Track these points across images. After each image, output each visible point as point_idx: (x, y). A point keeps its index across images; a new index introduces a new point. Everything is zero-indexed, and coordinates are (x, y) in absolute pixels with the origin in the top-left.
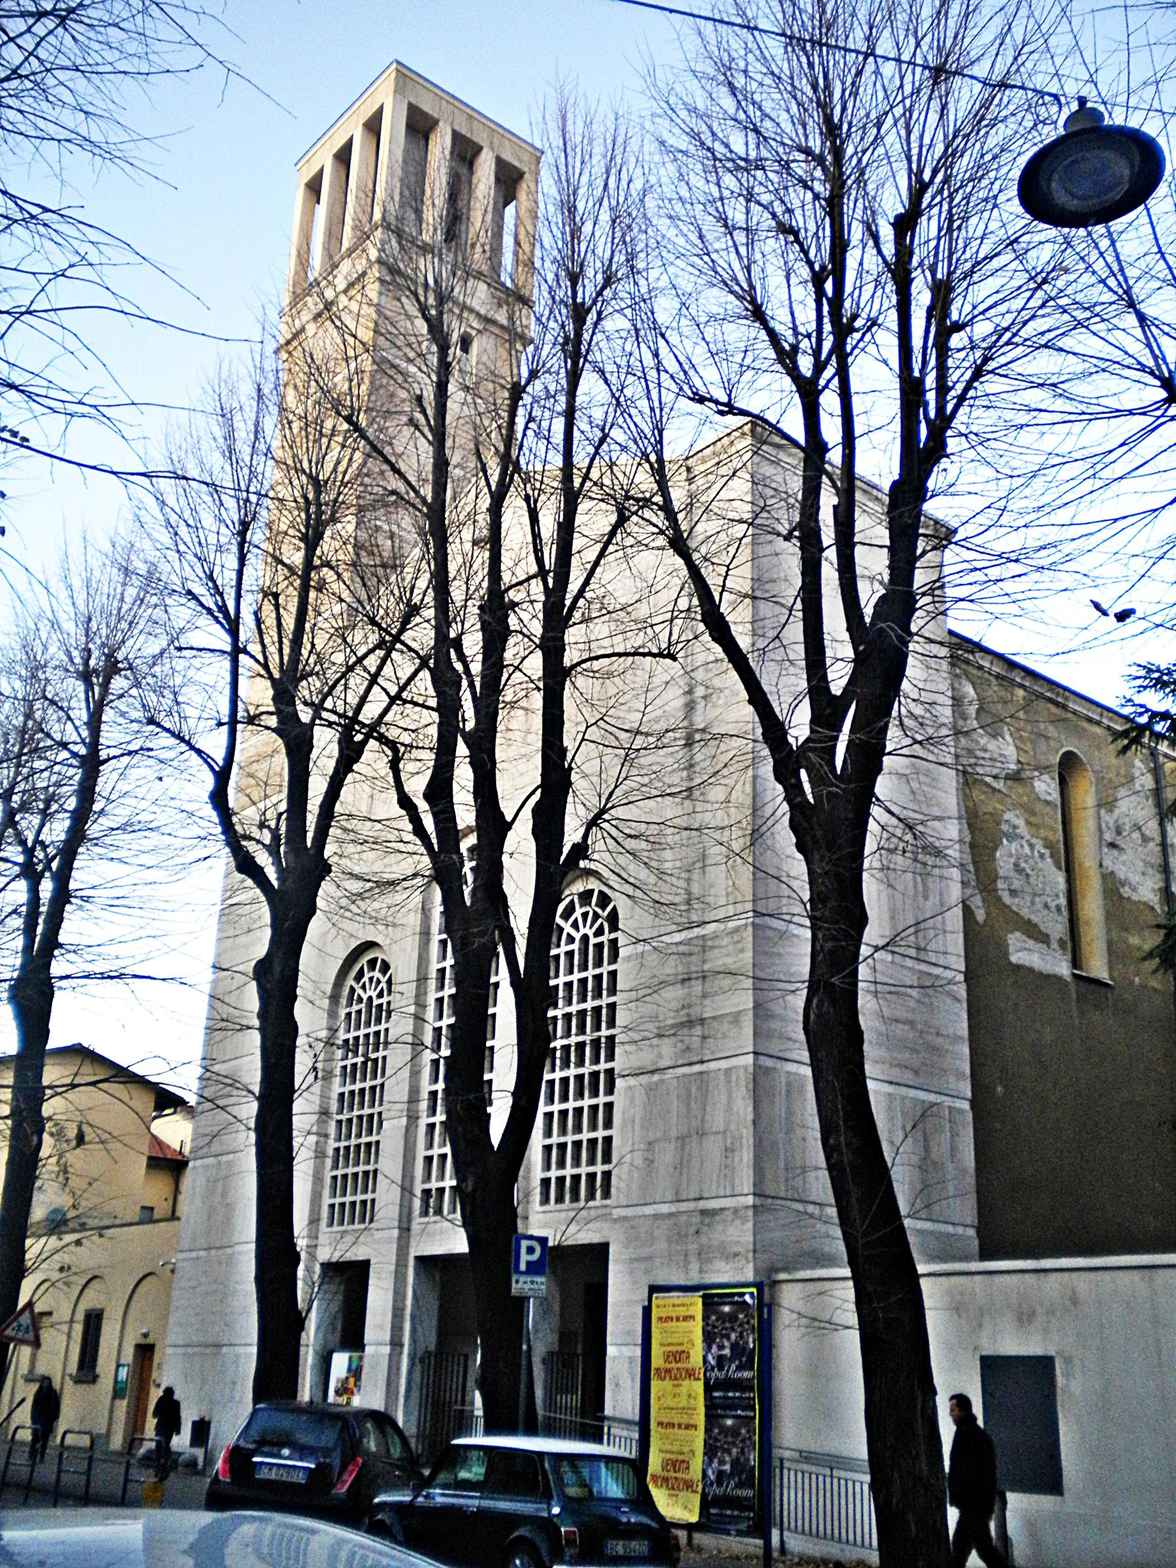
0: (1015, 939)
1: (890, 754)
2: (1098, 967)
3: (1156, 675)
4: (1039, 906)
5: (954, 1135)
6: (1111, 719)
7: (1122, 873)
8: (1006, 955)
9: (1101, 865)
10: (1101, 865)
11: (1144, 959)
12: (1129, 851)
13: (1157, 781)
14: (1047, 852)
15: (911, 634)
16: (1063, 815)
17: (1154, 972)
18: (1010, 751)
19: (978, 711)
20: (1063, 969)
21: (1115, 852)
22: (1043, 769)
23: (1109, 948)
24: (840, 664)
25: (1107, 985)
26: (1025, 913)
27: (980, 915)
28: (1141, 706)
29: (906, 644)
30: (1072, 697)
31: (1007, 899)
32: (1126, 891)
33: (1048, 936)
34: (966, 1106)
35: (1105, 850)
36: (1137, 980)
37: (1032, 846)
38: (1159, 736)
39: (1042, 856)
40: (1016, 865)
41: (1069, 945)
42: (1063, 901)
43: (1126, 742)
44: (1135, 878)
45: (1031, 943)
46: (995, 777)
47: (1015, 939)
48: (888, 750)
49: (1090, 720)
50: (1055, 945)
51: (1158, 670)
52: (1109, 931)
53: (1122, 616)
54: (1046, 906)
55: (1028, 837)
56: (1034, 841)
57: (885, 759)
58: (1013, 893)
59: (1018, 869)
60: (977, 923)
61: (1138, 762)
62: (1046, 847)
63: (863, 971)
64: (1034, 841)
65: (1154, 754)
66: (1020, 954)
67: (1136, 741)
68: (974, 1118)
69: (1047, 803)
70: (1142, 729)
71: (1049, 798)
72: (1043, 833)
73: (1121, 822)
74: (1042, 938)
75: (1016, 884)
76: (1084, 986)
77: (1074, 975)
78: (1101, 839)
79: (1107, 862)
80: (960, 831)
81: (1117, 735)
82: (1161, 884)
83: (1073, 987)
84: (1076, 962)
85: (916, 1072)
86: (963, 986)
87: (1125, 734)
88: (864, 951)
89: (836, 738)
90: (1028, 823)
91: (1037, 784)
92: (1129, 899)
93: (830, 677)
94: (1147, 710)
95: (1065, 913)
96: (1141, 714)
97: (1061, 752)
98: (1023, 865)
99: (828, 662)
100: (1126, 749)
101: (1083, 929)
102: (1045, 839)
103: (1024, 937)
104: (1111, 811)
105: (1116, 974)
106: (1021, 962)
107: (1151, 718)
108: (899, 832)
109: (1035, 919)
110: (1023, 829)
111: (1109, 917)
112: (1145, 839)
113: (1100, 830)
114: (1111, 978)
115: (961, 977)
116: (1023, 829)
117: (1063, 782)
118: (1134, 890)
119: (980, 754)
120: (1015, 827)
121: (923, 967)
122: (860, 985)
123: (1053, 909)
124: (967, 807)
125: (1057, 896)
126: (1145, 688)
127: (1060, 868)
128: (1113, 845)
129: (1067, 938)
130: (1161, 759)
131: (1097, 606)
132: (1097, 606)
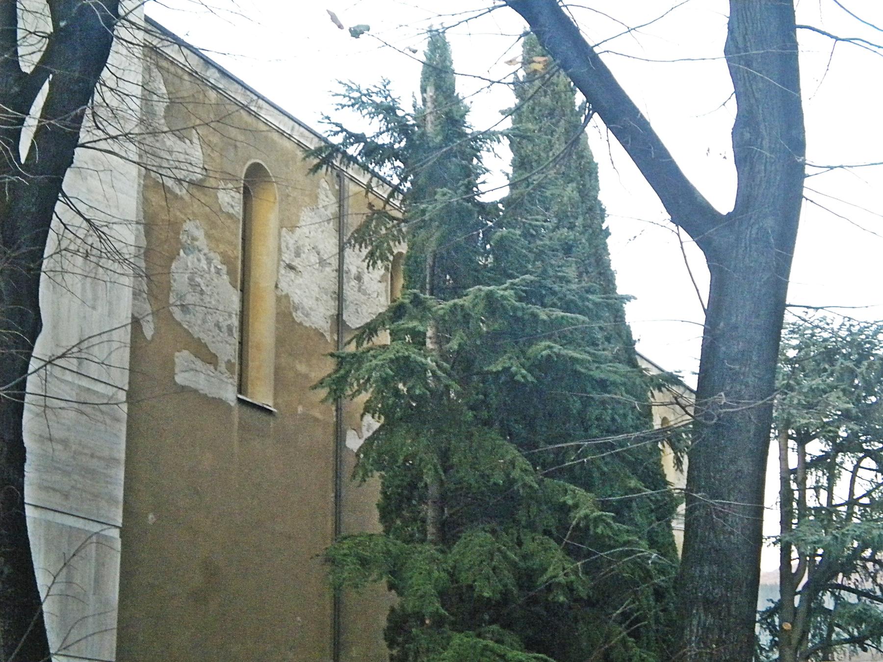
0: (182, 358)
1: (83, 146)
2: (263, 396)
3: (356, 95)
4: (210, 324)
5: (101, 564)
6: (302, 135)
7: (297, 296)
8: (173, 374)
9: (276, 287)
10: (276, 287)
11: (314, 387)
12: (306, 275)
13: (341, 206)
14: (224, 268)
15: (118, 16)
16: (244, 231)
17: (323, 401)
18: (196, 153)
19: (168, 109)
20: (230, 394)
21: (292, 274)
22: (229, 177)
23: (276, 373)
24: (34, 39)
25: (270, 412)
26: (197, 332)
27: (148, 330)
28: (337, 125)
29: (111, 26)
30: (265, 105)
31: (178, 314)
32: (298, 316)
33: (215, 356)
34: (115, 533)
35: (283, 271)
36: (300, 409)
37: (209, 261)
38: (352, 159)
39: (218, 271)
40: (191, 279)
41: (237, 367)
42: (235, 321)
43: (316, 161)
44: (308, 303)
45: (199, 364)
46: (179, 181)
47: (182, 358)
48: (81, 141)
49: (282, 133)
50: (222, 367)
51: (358, 90)
52: (277, 356)
53: (356, 33)
54: (218, 326)
55: (206, 251)
56: (212, 255)
57: (78, 151)
58: (184, 308)
59: (193, 284)
60: (145, 338)
61: (324, 181)
62: (223, 263)
63: (32, 384)
64: (212, 255)
65: (340, 176)
66: (186, 375)
67: (327, 161)
68: (123, 545)
69: (230, 216)
70: (335, 149)
71: (231, 211)
72: (222, 247)
73: (300, 243)
74: (211, 359)
75: (190, 299)
76: (248, 411)
77: (239, 399)
78: (280, 259)
79: (283, 285)
80: (137, 237)
81: (309, 153)
82: (334, 312)
83: (236, 413)
84: (241, 388)
85: (66, 496)
86: (125, 407)
87: (319, 151)
88: (33, 365)
89: (22, 122)
90: (208, 236)
91: (221, 194)
92: (301, 324)
93: (21, 51)
94: (343, 130)
95: (236, 335)
96: (336, 133)
97: (249, 163)
98: (198, 280)
99: (20, 34)
100: (317, 167)
101: (252, 352)
102: (223, 255)
103: (193, 358)
104: (293, 232)
105: (280, 401)
106: (187, 383)
107: (346, 138)
108: (81, 233)
109: (205, 338)
110: (202, 242)
111: (280, 342)
112: (322, 262)
113: (280, 249)
114: (276, 405)
115: (122, 396)
116: (202, 242)
117: (247, 194)
118: (307, 315)
119: (164, 154)
120: (194, 239)
121: (85, 383)
122: (28, 398)
123: (225, 329)
124: (145, 212)
125: (230, 316)
126: (343, 106)
127: (235, 287)
128: (291, 267)
129: (235, 361)
130: (347, 181)
131: (334, 19)
132: (334, 19)
